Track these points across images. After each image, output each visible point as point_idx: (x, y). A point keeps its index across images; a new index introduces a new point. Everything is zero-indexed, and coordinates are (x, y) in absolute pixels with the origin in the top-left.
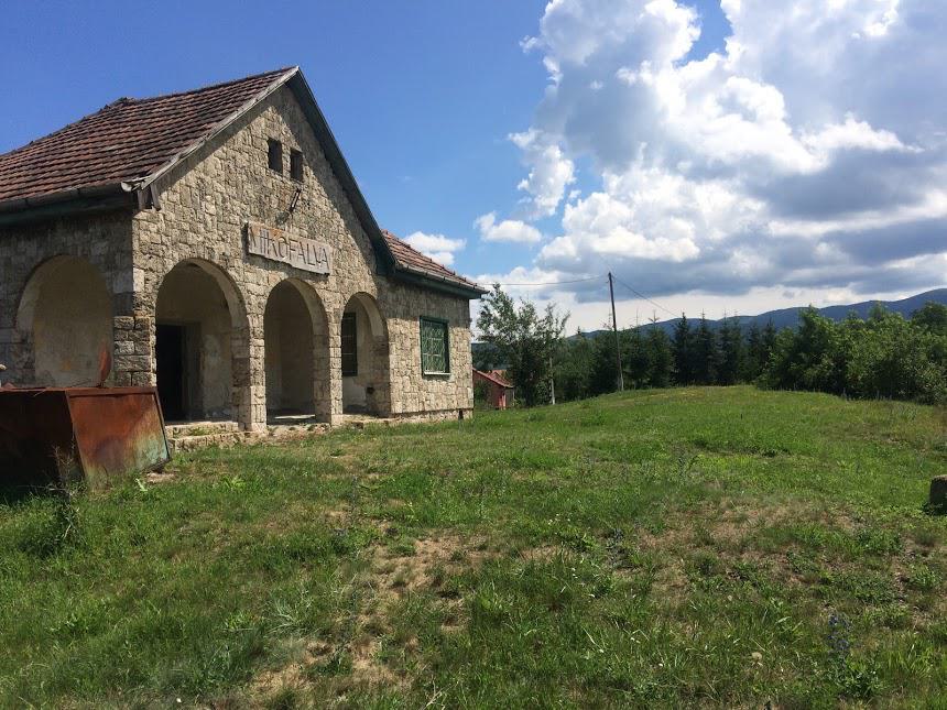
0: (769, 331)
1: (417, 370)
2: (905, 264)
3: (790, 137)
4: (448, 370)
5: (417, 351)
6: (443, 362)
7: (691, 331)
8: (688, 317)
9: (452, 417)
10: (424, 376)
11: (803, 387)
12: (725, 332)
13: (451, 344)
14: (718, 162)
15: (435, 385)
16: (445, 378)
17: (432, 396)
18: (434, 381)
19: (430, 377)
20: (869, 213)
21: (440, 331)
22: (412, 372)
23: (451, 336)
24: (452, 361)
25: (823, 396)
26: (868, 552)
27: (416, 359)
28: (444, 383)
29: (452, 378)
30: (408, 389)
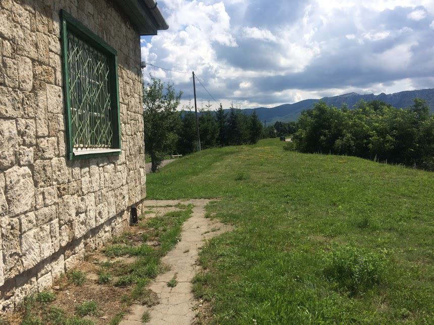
0: (254, 116)
1: (53, 146)
2: (278, 94)
3: (169, 21)
4: (116, 143)
5: (52, 98)
6: (106, 128)
7: (224, 115)
8: (224, 108)
9: (120, 225)
10: (72, 160)
11: (335, 152)
12: (186, 120)
13: (120, 92)
14: (420, 10)
15: (96, 176)
16: (110, 158)
17: (90, 199)
18: (94, 168)
19: (85, 161)
20: (252, 70)
21: (101, 66)
22: (40, 153)
23: (120, 83)
24: (123, 128)
25: (357, 159)
26: (11, 233)
27: (51, 118)
28: (110, 167)
29: (122, 158)
30: (25, 201)
